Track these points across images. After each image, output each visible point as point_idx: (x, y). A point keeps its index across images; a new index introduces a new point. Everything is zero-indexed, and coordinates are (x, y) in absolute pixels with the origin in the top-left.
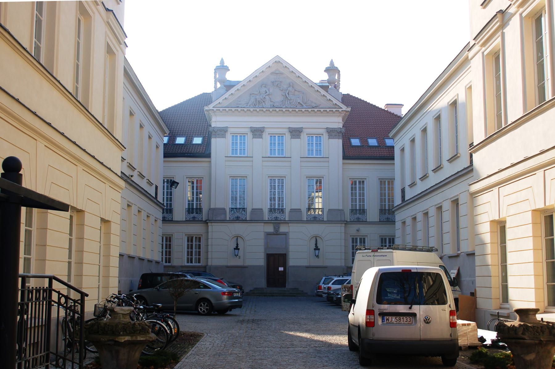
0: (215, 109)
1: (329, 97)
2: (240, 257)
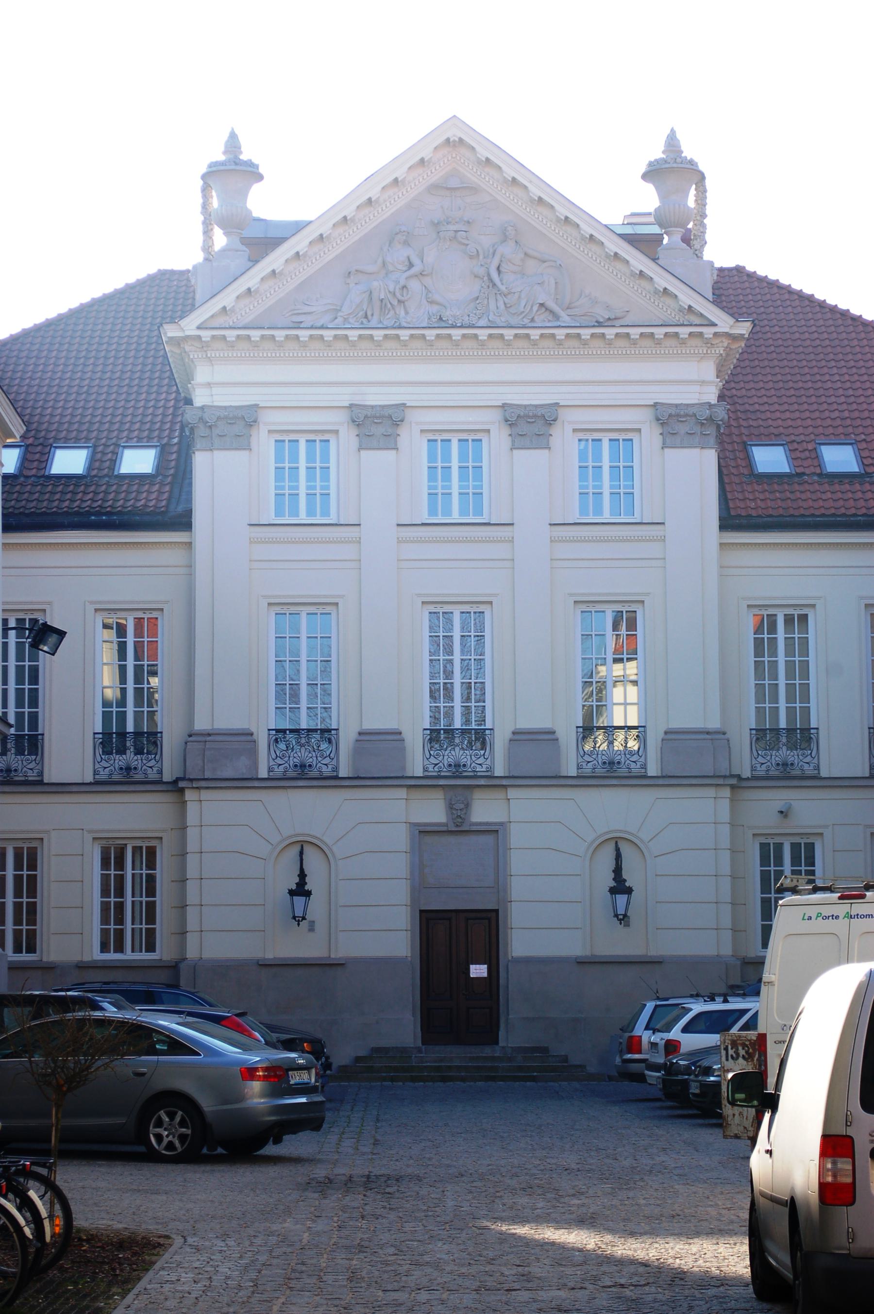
0: (206, 335)
1: (662, 281)
2: (312, 923)
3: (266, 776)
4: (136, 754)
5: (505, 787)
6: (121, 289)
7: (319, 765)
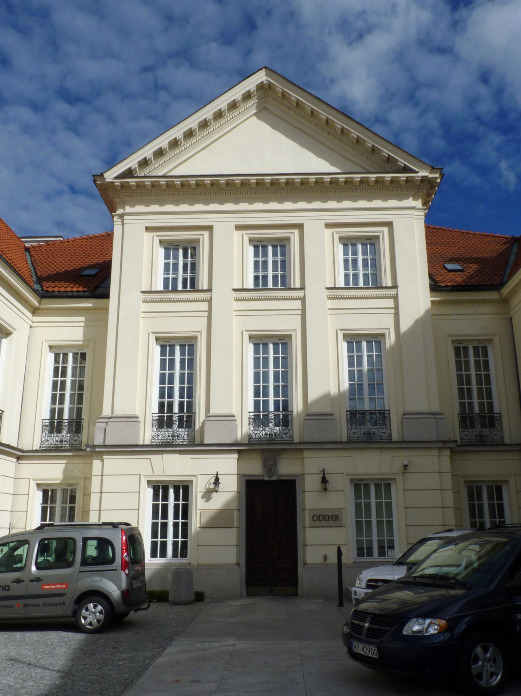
3: (149, 443)
5: (302, 450)
6: (197, 203)
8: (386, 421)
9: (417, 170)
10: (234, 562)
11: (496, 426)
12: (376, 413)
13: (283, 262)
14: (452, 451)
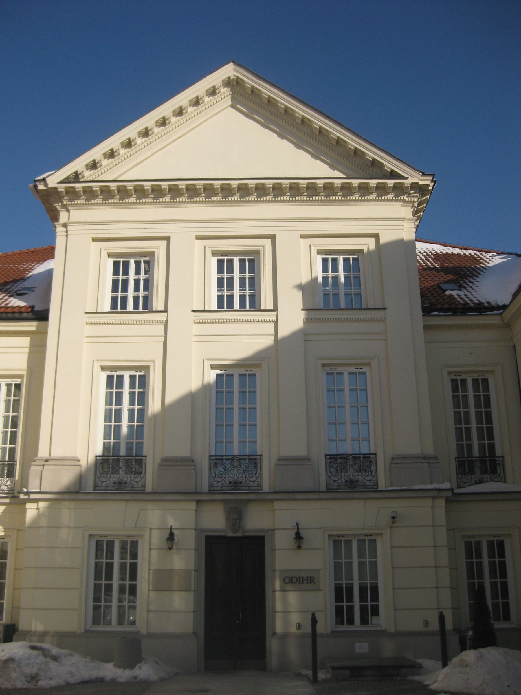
4: (126, 473)
5: (272, 501)
7: (248, 482)
8: (372, 467)
9: (406, 176)
10: (192, 631)
11: (499, 471)
12: (360, 457)
13: (252, 279)
14: (448, 501)
